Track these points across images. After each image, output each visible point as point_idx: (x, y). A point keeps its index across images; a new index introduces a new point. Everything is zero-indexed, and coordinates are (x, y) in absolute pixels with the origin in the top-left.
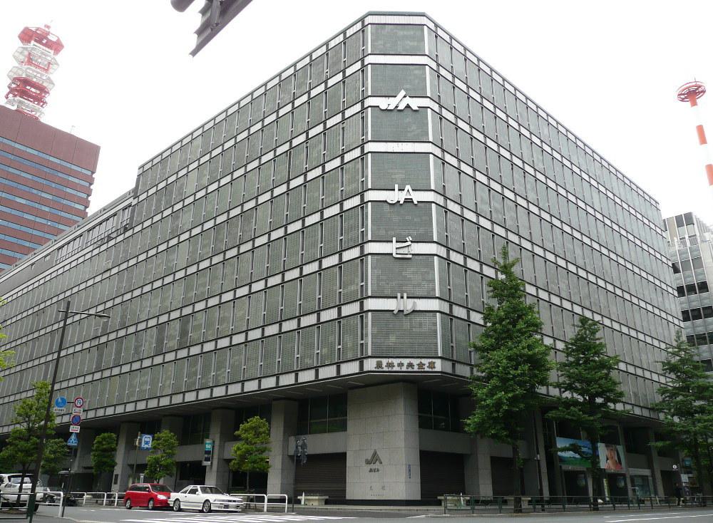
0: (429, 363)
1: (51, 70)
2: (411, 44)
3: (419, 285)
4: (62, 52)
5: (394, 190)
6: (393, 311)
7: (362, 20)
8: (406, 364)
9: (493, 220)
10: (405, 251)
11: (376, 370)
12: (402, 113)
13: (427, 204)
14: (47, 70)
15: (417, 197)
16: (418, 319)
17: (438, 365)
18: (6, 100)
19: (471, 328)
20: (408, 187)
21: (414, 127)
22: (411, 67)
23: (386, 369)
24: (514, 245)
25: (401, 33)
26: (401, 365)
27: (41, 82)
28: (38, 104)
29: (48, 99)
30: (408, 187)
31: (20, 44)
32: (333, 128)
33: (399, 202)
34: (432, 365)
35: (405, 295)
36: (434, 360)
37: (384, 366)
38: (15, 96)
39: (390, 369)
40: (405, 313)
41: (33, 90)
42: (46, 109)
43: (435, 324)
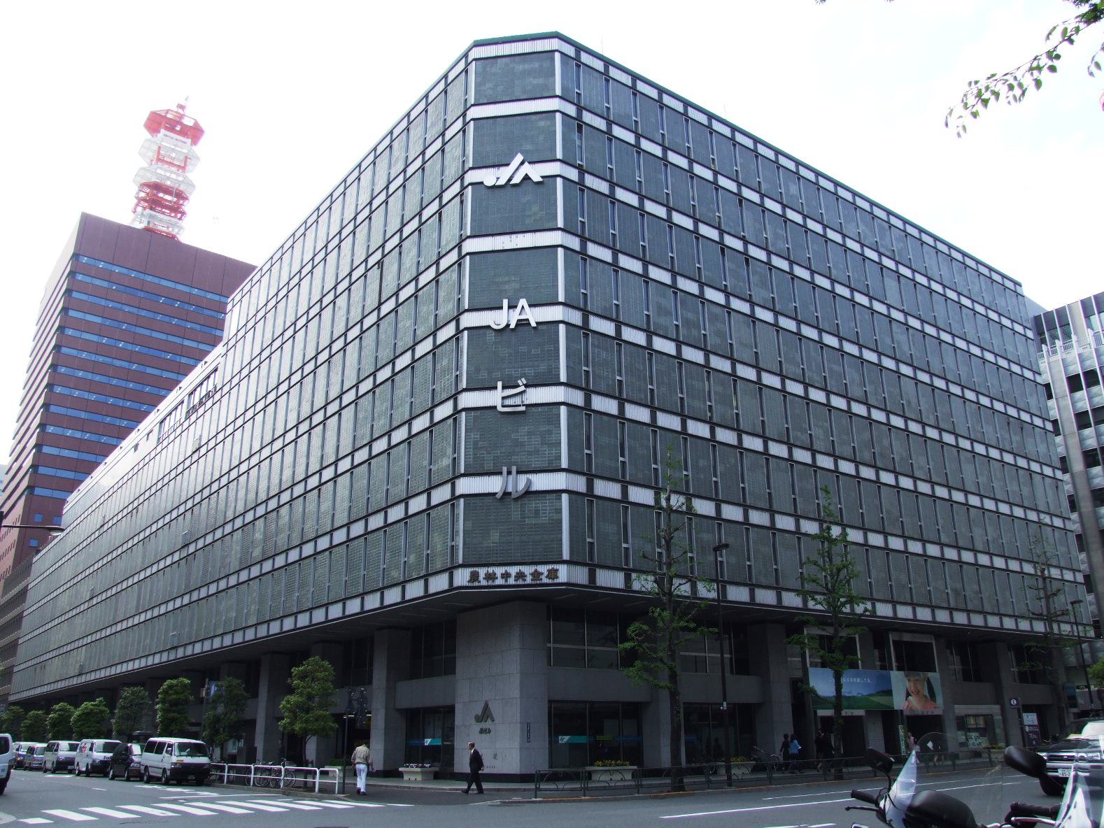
0: (549, 571)
1: (189, 167)
2: (535, 82)
3: (537, 452)
4: (203, 141)
5: (501, 308)
6: (496, 493)
7: (466, 55)
8: (513, 574)
9: (841, 335)
10: (517, 400)
11: (470, 584)
12: (519, 190)
13: (552, 326)
14: (183, 168)
15: (535, 316)
16: (533, 504)
17: (563, 573)
18: (133, 215)
19: (1006, 469)
20: (523, 302)
21: (535, 208)
22: (533, 117)
23: (484, 583)
24: (722, 375)
25: (520, 67)
26: (506, 576)
27: (176, 186)
28: (176, 217)
29: (187, 207)
30: (523, 302)
31: (146, 134)
32: (428, 222)
33: (508, 325)
34: (553, 574)
35: (514, 469)
36: (556, 566)
37: (481, 578)
38: (145, 208)
39: (490, 583)
40: (513, 496)
41: (168, 197)
42: (185, 222)
43: (559, 511)
